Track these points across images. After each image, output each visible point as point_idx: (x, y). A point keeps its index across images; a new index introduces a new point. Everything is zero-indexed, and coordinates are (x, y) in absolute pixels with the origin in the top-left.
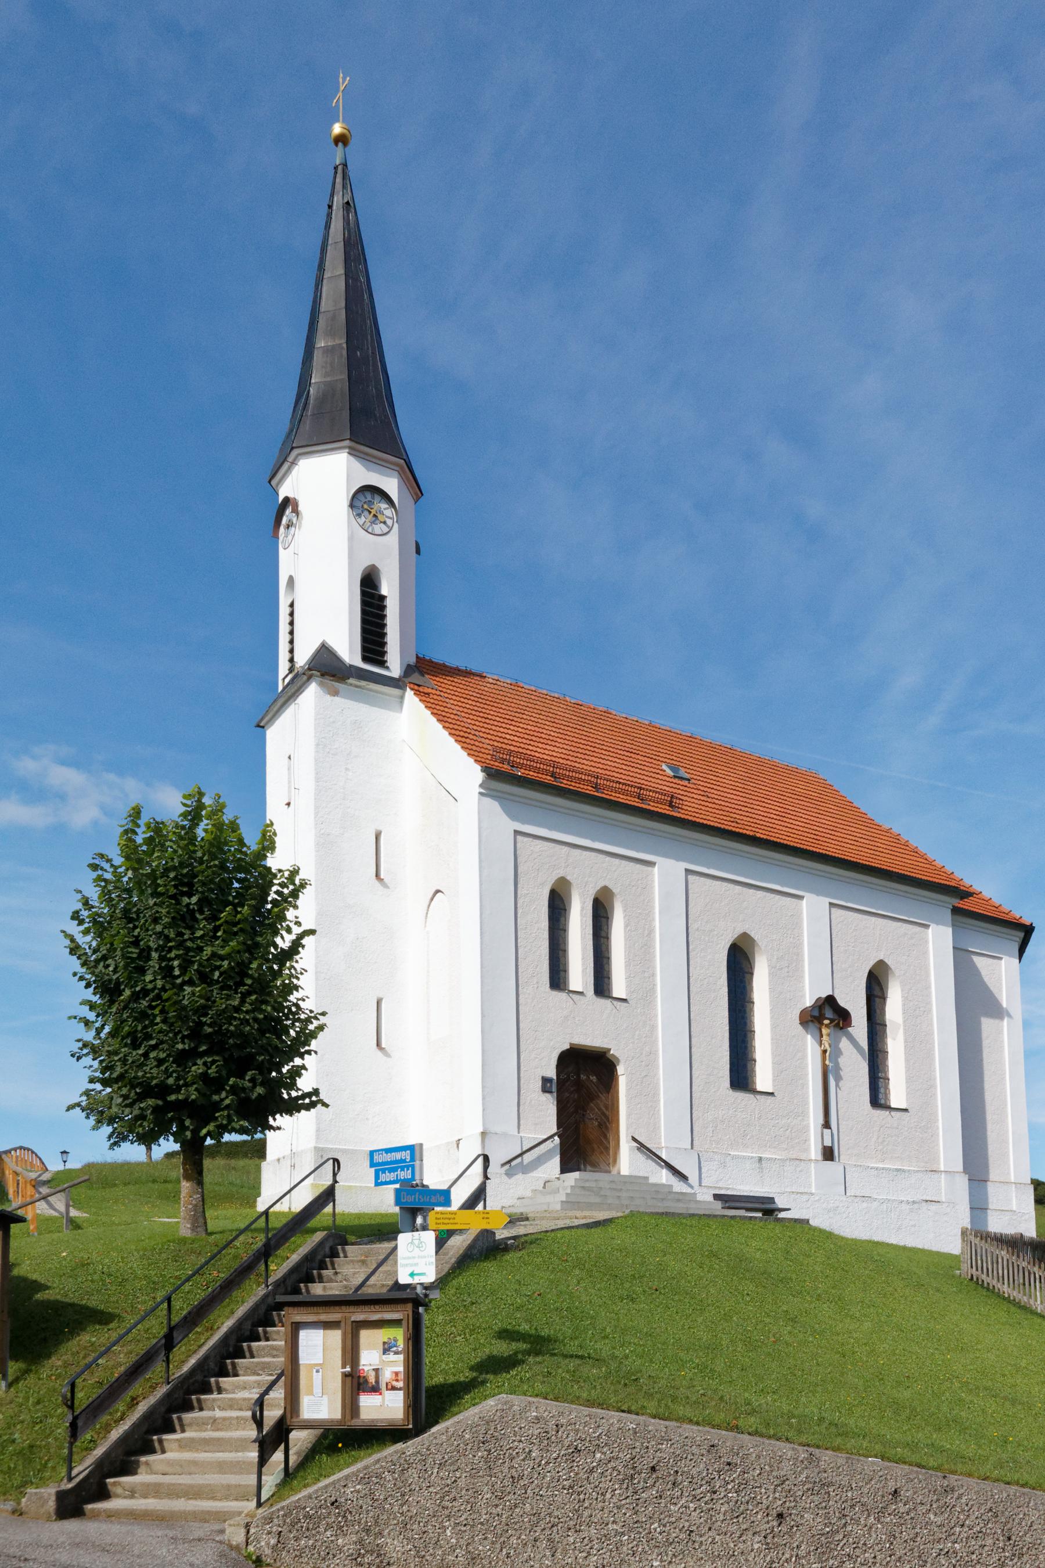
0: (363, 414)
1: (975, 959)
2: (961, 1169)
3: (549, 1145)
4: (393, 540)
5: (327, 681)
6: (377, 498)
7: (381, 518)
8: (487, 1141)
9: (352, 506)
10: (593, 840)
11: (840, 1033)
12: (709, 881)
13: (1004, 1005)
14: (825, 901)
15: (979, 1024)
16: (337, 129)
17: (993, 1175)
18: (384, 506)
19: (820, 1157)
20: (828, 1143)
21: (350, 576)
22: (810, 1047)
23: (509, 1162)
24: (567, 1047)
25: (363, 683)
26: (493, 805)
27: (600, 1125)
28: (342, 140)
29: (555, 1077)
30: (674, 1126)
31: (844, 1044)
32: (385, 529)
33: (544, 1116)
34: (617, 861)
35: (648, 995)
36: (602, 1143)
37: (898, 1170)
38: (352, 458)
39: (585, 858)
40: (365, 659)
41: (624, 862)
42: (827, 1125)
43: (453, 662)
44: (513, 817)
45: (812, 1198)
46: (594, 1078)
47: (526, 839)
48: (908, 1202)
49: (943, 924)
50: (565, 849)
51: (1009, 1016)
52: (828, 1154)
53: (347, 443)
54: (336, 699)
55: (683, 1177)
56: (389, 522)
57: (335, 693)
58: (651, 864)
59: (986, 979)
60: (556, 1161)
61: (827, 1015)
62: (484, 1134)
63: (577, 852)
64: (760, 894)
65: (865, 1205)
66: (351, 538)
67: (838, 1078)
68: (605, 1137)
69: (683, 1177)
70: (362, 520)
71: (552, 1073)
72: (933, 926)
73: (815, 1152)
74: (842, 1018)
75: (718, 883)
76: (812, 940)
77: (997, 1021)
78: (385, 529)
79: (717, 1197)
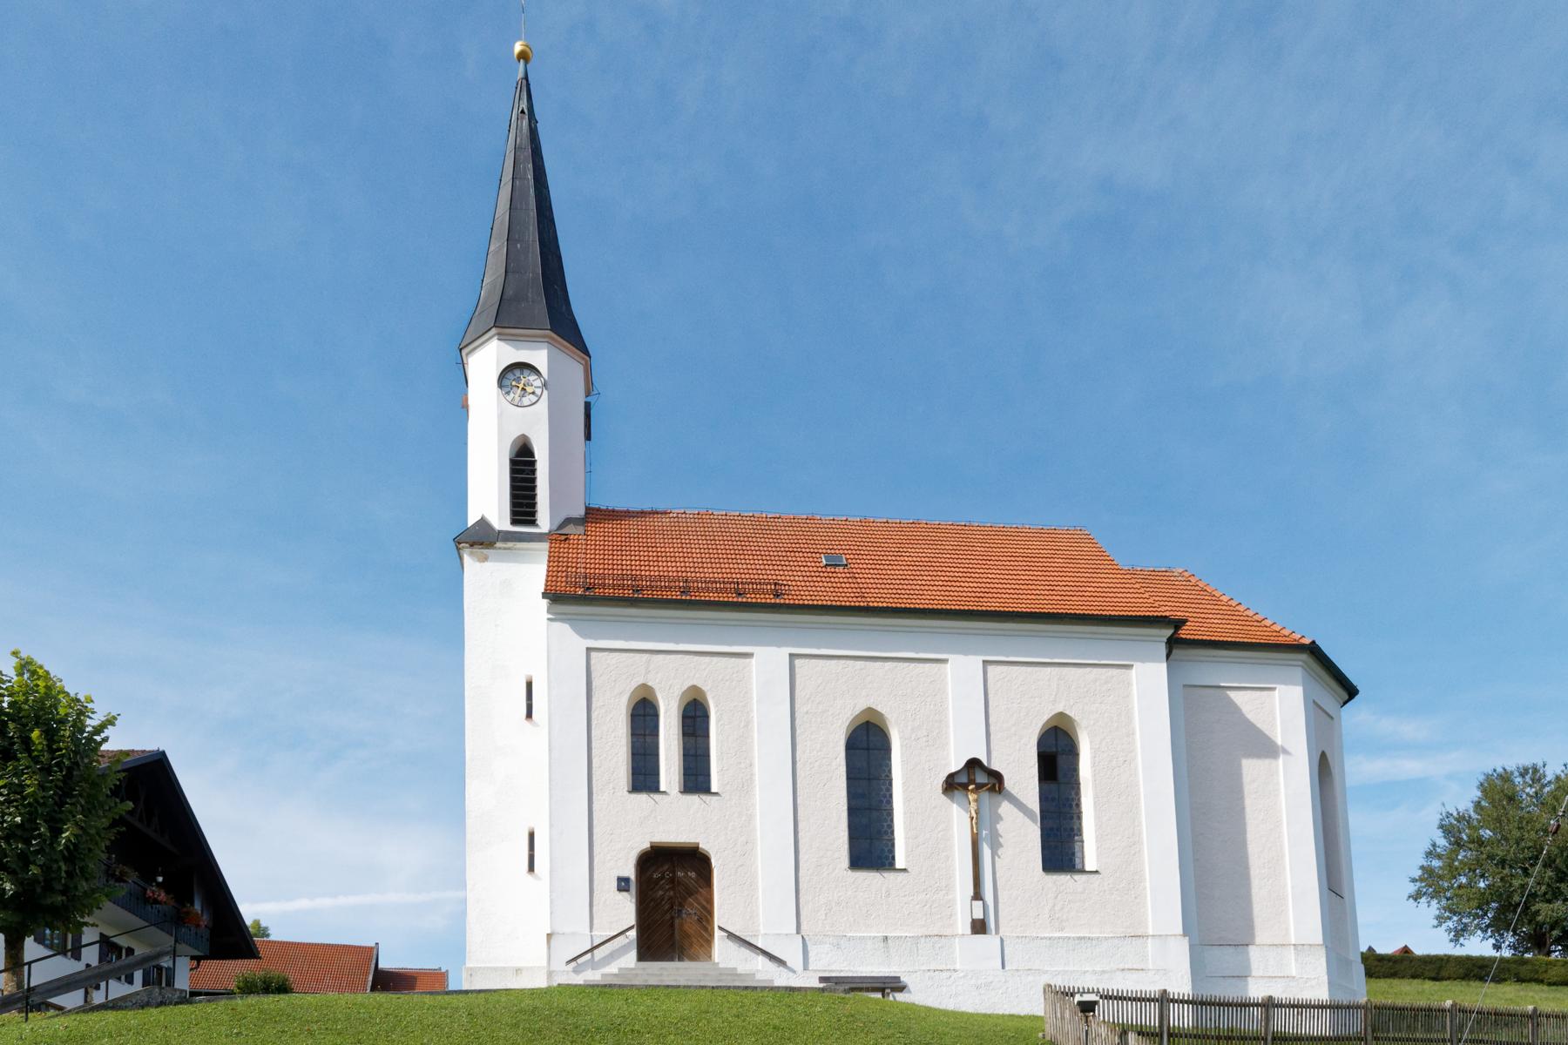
0: (539, 295)
1: (1232, 694)
2: (1180, 930)
3: (621, 940)
4: (543, 407)
5: (476, 550)
6: (526, 372)
7: (529, 389)
8: (553, 942)
9: (501, 384)
10: (626, 639)
11: (1000, 797)
12: (821, 662)
13: (1279, 742)
14: (975, 661)
15: (1240, 766)
16: (518, 47)
17: (1262, 935)
18: (532, 378)
19: (969, 931)
20: (979, 915)
21: (499, 451)
22: (958, 817)
23: (574, 959)
24: (646, 845)
25: (510, 544)
26: (564, 628)
27: (699, 921)
28: (523, 56)
29: (633, 877)
30: (783, 914)
31: (1005, 808)
32: (534, 398)
33: (624, 911)
34: (707, 659)
35: (745, 787)
36: (702, 936)
37: (1080, 938)
38: (502, 344)
39: (669, 662)
40: (514, 522)
41: (715, 659)
42: (978, 895)
43: (620, 505)
44: (583, 634)
45: (955, 975)
46: (693, 875)
47: (601, 654)
48: (1095, 972)
49: (1154, 660)
50: (646, 656)
51: (1285, 752)
52: (979, 927)
53: (494, 331)
54: (486, 564)
55: (781, 962)
56: (538, 391)
57: (485, 559)
58: (749, 655)
59: (1250, 716)
60: (633, 954)
61: (975, 780)
62: (549, 936)
63: (661, 657)
64: (888, 665)
65: (1030, 978)
66: (500, 416)
67: (996, 846)
68: (706, 929)
69: (781, 962)
70: (510, 398)
71: (630, 871)
72: (1138, 666)
73: (964, 926)
74: (996, 782)
75: (834, 662)
76: (957, 703)
77: (1267, 762)
78: (534, 398)
79: (822, 979)
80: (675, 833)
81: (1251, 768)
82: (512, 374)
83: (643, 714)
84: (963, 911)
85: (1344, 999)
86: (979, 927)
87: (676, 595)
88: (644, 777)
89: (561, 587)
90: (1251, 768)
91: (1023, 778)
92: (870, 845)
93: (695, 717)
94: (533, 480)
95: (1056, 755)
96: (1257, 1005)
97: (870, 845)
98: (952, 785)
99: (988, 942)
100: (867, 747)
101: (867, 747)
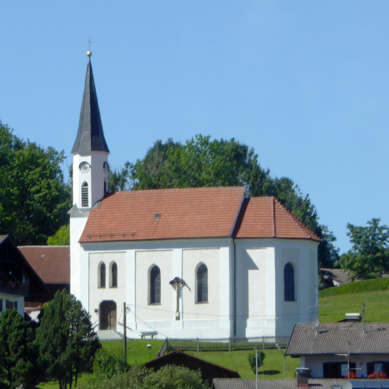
39: (108, 257)
42: (178, 310)
52: (178, 318)
71: (97, 307)
80: (108, 298)
81: (251, 273)
82: (82, 165)
83: (102, 267)
84: (175, 315)
85: (128, 346)
86: (178, 318)
87: (109, 238)
88: (102, 284)
89: (82, 241)
90: (251, 273)
91: (191, 280)
92: (154, 297)
93: (114, 267)
94: (87, 198)
95: (202, 271)
96: (261, 338)
97: (154, 297)
98: (172, 283)
99: (180, 322)
100: (155, 273)
101: (155, 273)
